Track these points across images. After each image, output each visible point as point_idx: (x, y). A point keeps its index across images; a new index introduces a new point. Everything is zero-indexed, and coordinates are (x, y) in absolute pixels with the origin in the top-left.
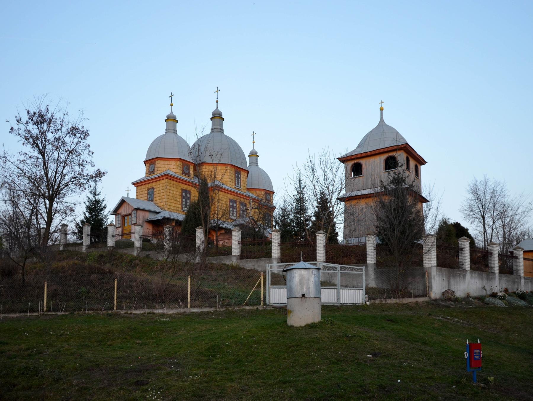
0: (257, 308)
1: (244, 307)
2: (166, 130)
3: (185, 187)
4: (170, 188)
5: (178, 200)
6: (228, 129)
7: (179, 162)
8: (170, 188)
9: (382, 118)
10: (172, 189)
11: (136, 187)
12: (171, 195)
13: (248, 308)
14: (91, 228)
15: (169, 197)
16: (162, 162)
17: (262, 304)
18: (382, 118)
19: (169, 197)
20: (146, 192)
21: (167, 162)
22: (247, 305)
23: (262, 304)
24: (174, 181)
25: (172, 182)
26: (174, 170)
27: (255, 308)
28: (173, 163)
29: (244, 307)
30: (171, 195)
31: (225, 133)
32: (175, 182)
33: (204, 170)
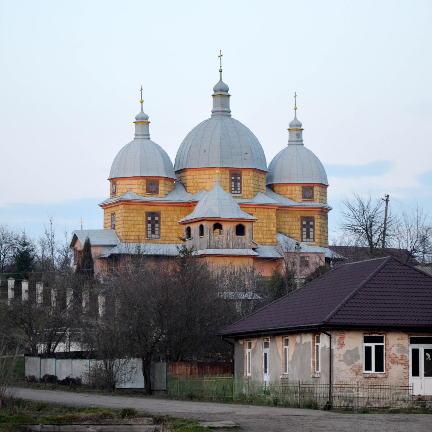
2: (135, 135)
3: (151, 209)
4: (128, 215)
5: (141, 226)
6: (238, 110)
7: (141, 181)
8: (128, 215)
9: (221, 79)
10: (132, 215)
11: (104, 209)
12: (129, 222)
14: (15, 282)
15: (127, 226)
16: (122, 182)
18: (221, 79)
19: (127, 226)
20: (110, 217)
21: (128, 182)
24: (134, 205)
25: (132, 207)
26: (136, 191)
28: (135, 182)
30: (129, 222)
31: (234, 115)
32: (135, 207)
33: (189, 177)
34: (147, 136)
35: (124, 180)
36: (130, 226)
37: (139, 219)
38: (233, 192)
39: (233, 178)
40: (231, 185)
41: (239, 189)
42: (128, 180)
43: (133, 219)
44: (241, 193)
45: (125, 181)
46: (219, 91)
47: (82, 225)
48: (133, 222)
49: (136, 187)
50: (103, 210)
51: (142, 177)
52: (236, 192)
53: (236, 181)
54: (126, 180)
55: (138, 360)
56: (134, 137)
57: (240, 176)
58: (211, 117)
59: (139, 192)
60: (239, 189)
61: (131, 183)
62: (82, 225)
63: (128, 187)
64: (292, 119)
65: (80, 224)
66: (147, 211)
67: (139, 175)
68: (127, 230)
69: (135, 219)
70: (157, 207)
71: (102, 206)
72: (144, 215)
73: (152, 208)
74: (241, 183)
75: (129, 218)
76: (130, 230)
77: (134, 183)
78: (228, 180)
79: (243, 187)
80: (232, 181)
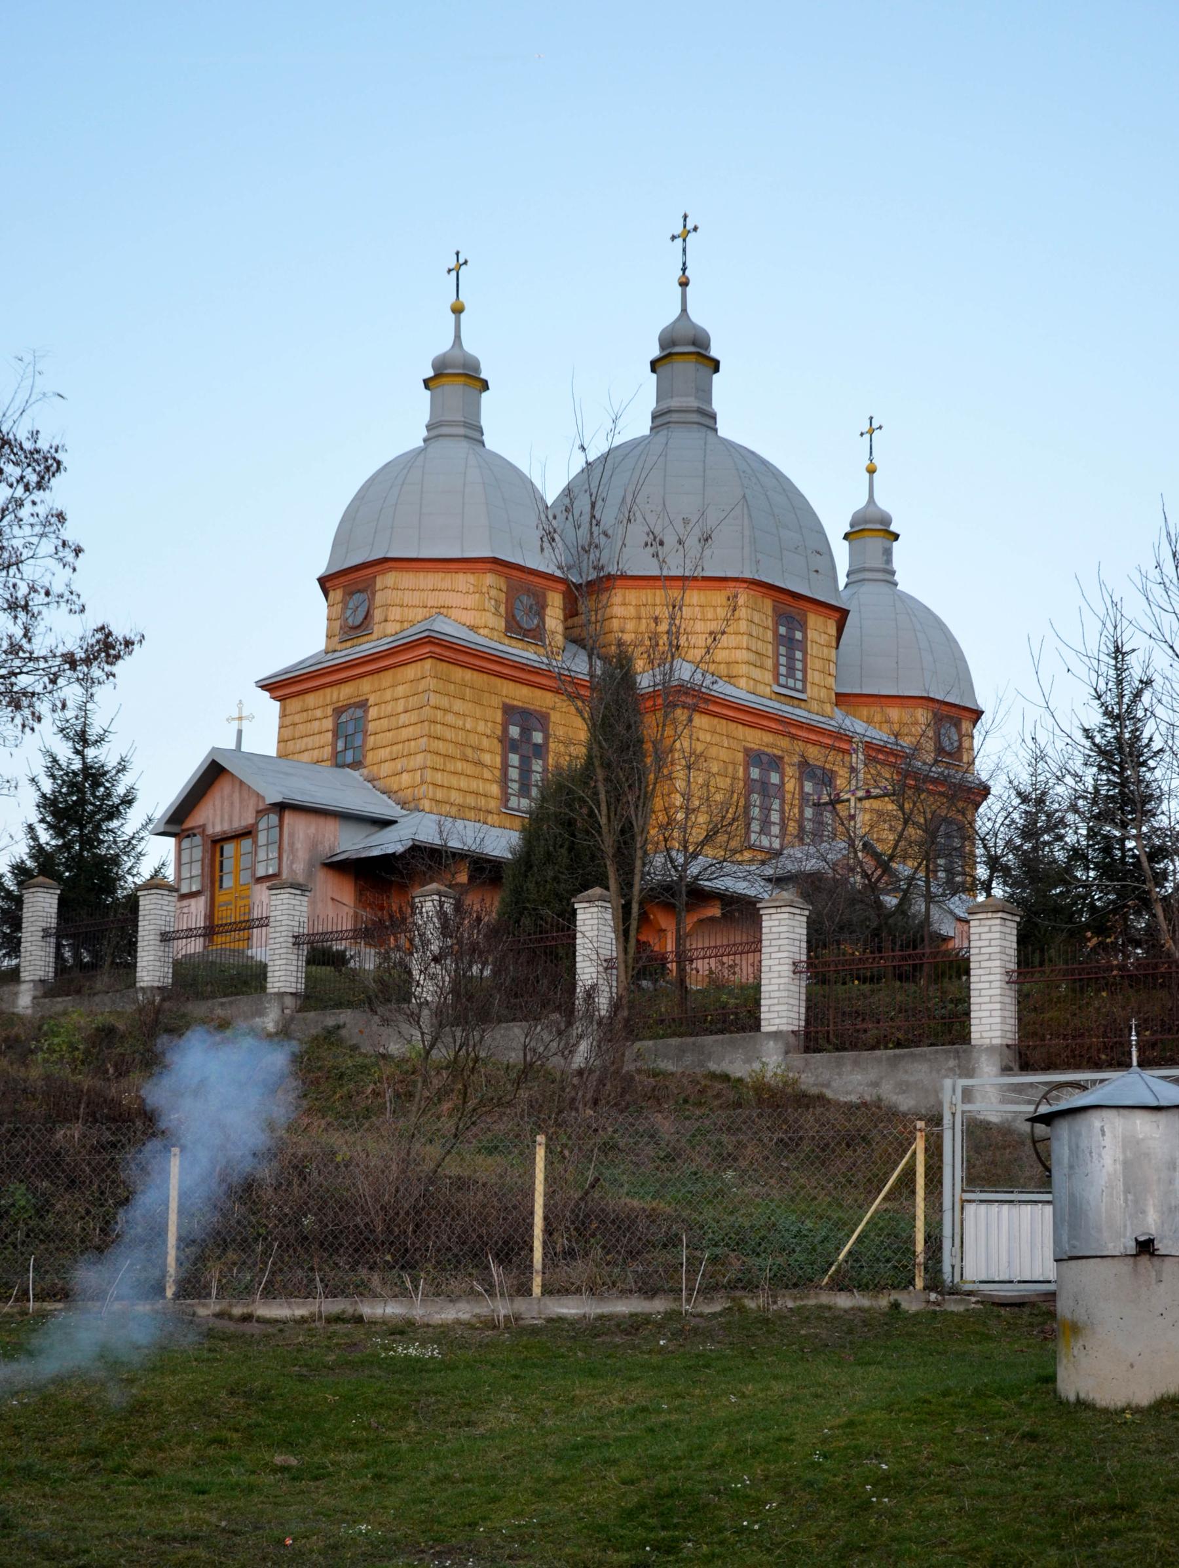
0: (896, 1305)
1: (825, 1299)
3: (521, 695)
4: (444, 702)
7: (490, 579)
8: (444, 702)
9: (684, 310)
10: (458, 706)
12: (449, 734)
13: (843, 1301)
14: (62, 902)
15: (440, 746)
16: (406, 579)
17: (919, 1283)
18: (684, 310)
19: (440, 746)
20: (329, 724)
22: (839, 1285)
23: (919, 1283)
25: (458, 674)
27: (884, 1302)
28: (463, 581)
29: (825, 1299)
30: (449, 734)
32: (468, 675)
33: (618, 611)
34: (474, 433)
35: (417, 570)
36: (451, 749)
37: (481, 727)
38: (782, 680)
39: (782, 630)
40: (777, 654)
41: (799, 675)
42: (436, 571)
43: (460, 723)
44: (803, 691)
45: (422, 575)
46: (687, 344)
47: (240, 732)
48: (461, 737)
49: (471, 601)
50: (278, 703)
51: (496, 564)
52: (791, 682)
53: (790, 643)
54: (428, 570)
55: (1088, 1394)
56: (424, 433)
57: (803, 627)
58: (647, 432)
59: (481, 622)
60: (799, 675)
61: (447, 584)
62: (240, 732)
63: (433, 599)
64: (862, 502)
65: (235, 725)
66: (507, 701)
67: (486, 553)
68: (439, 762)
69: (468, 726)
70: (539, 692)
71: (263, 687)
72: (499, 717)
73: (525, 691)
74: (805, 653)
75: (450, 719)
76: (450, 766)
77: (462, 587)
78: (769, 635)
79: (809, 671)
80: (779, 639)
